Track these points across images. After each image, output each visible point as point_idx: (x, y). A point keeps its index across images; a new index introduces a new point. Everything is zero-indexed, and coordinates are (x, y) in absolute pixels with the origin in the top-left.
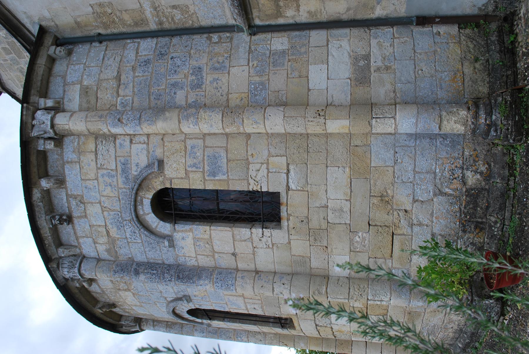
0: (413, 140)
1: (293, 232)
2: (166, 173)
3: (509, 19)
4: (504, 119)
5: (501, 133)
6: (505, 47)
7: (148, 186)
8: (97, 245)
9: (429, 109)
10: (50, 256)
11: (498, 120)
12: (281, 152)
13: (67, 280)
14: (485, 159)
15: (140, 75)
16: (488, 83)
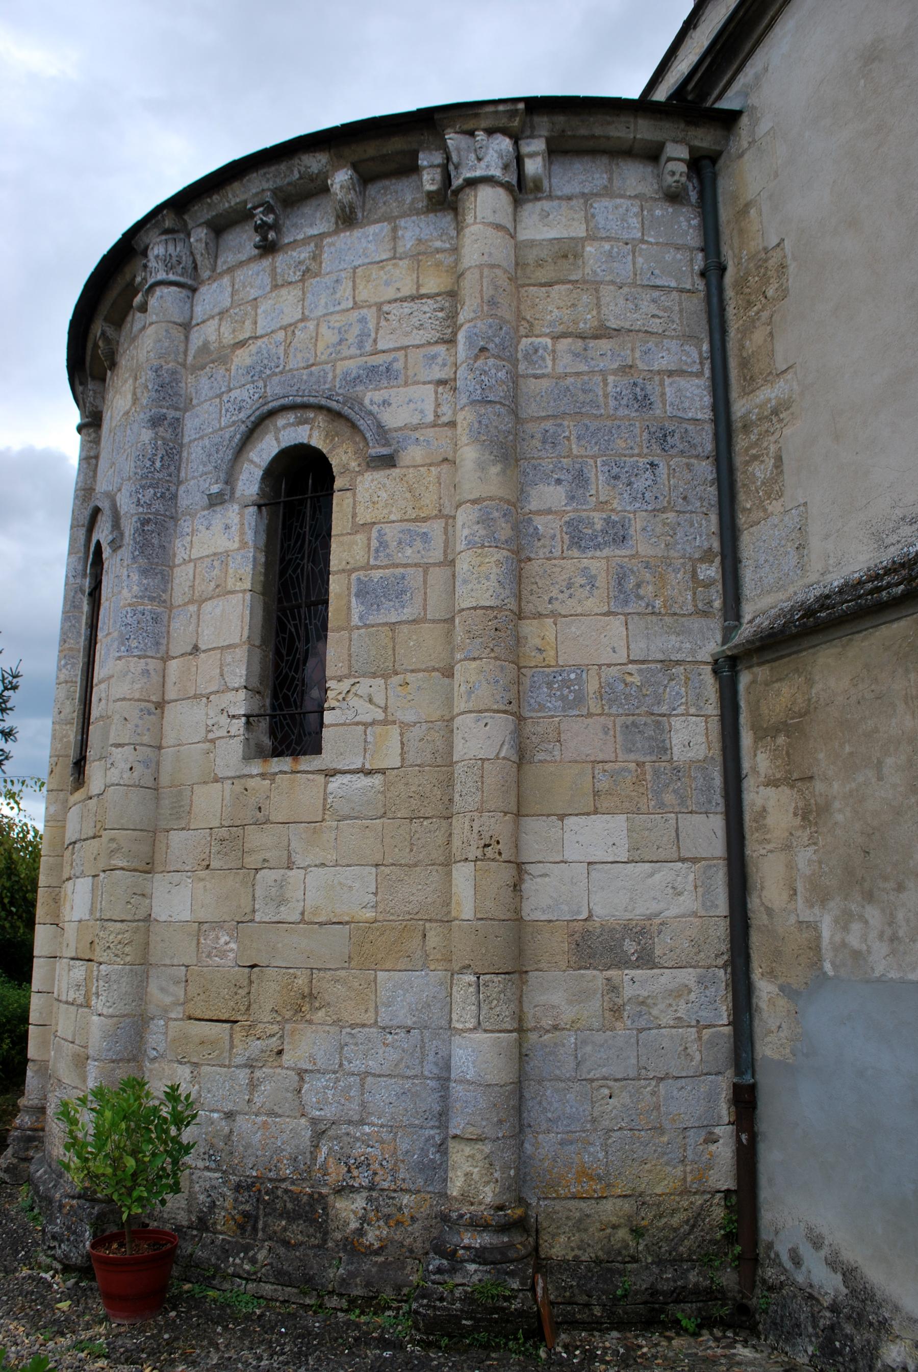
0: (436, 1071)
2: (366, 475)
3: (744, 1318)
4: (466, 1292)
5: (434, 1282)
6: (667, 1304)
7: (337, 435)
8: (217, 318)
9: (498, 1113)
10: (189, 210)
11: (464, 1277)
12: (411, 753)
13: (145, 253)
14: (392, 1241)
15: (610, 388)
16: (576, 1258)
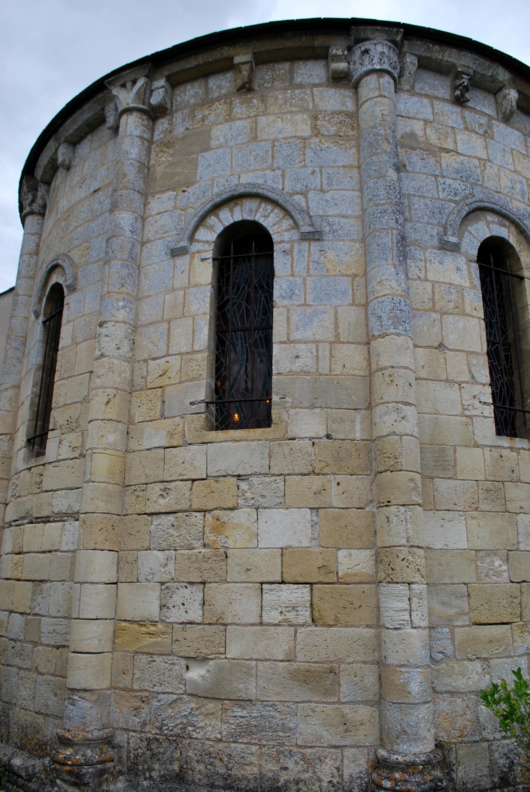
1: (496, 453)
